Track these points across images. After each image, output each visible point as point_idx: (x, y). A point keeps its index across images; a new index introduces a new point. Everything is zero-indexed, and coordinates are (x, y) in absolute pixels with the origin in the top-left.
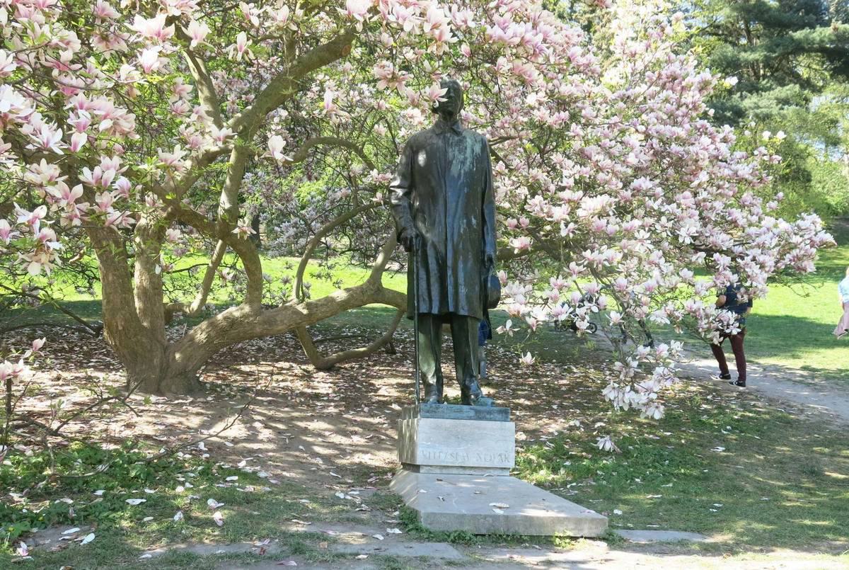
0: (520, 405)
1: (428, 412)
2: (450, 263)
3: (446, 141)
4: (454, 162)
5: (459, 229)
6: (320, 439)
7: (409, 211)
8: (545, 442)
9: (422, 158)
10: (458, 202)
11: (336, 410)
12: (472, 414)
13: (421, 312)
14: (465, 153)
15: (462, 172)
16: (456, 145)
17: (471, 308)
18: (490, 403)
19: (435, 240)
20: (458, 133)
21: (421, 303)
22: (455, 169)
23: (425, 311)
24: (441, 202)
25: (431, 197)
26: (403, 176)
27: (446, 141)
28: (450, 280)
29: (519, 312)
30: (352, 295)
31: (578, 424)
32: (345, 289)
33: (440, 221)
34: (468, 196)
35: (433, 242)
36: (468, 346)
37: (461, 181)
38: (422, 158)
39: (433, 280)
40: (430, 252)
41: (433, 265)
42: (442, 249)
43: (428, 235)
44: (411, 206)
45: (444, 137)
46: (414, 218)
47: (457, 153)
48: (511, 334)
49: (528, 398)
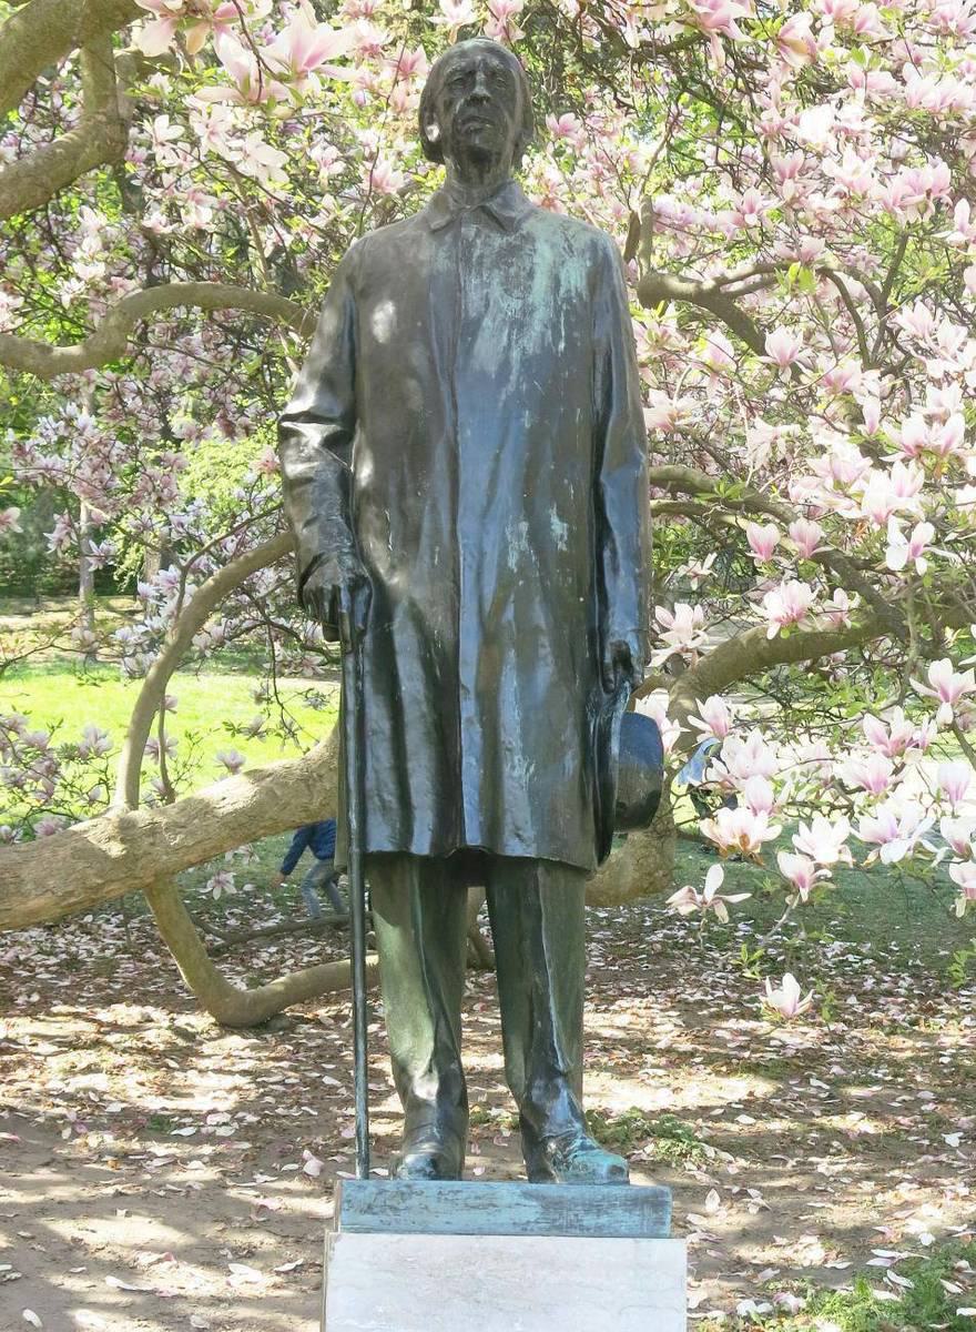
0: (840, 1134)
1: (369, 1209)
2: (468, 675)
3: (464, 255)
4: (487, 322)
5: (504, 555)
6: (113, 1281)
7: (337, 498)
8: (882, 1272)
9: (382, 319)
10: (497, 458)
11: (211, 1174)
12: (531, 1211)
13: (373, 848)
14: (528, 289)
15: (515, 355)
16: (495, 265)
17: (548, 833)
18: (604, 1171)
19: (418, 594)
20: (502, 225)
22: (487, 349)
23: (388, 847)
25: (411, 453)
26: (328, 382)
27: (464, 255)
28: (470, 737)
29: (744, 838)
30: (270, 792)
32: (248, 774)
33: (437, 530)
34: (535, 438)
35: (413, 604)
36: (541, 968)
37: (511, 388)
38: (382, 319)
39: (415, 736)
40: (404, 638)
41: (412, 683)
42: (438, 620)
43: (396, 581)
44: (346, 481)
45: (457, 237)
46: (353, 523)
47: (496, 291)
48: (722, 912)
49: (873, 1109)
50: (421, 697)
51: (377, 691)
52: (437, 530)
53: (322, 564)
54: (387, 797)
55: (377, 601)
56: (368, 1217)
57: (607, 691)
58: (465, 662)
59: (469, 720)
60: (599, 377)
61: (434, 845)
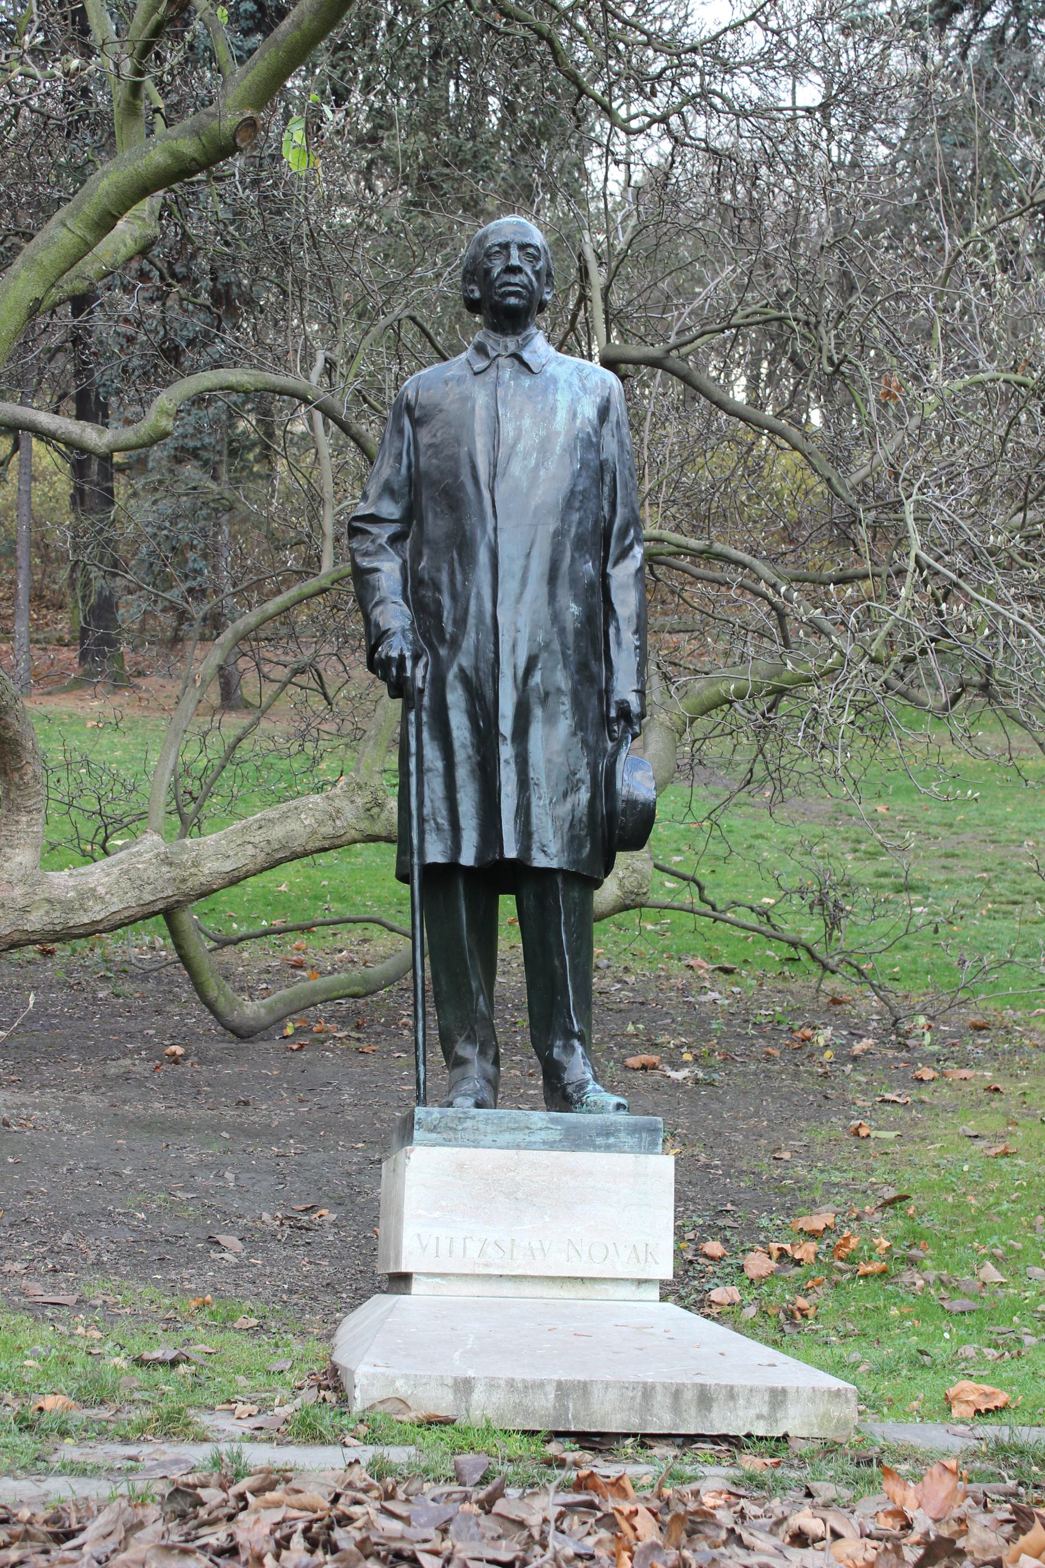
12: (441, 1141)
21: (431, 838)
23: (441, 860)
24: (483, 556)
31: (179, 1194)
39: (463, 774)
50: (468, 743)
51: (433, 738)
52: (480, 619)
53: (389, 637)
54: (440, 821)
55: (433, 665)
56: (434, 1135)
57: (612, 740)
58: (504, 717)
59: (507, 762)
60: (606, 489)
61: (478, 858)
